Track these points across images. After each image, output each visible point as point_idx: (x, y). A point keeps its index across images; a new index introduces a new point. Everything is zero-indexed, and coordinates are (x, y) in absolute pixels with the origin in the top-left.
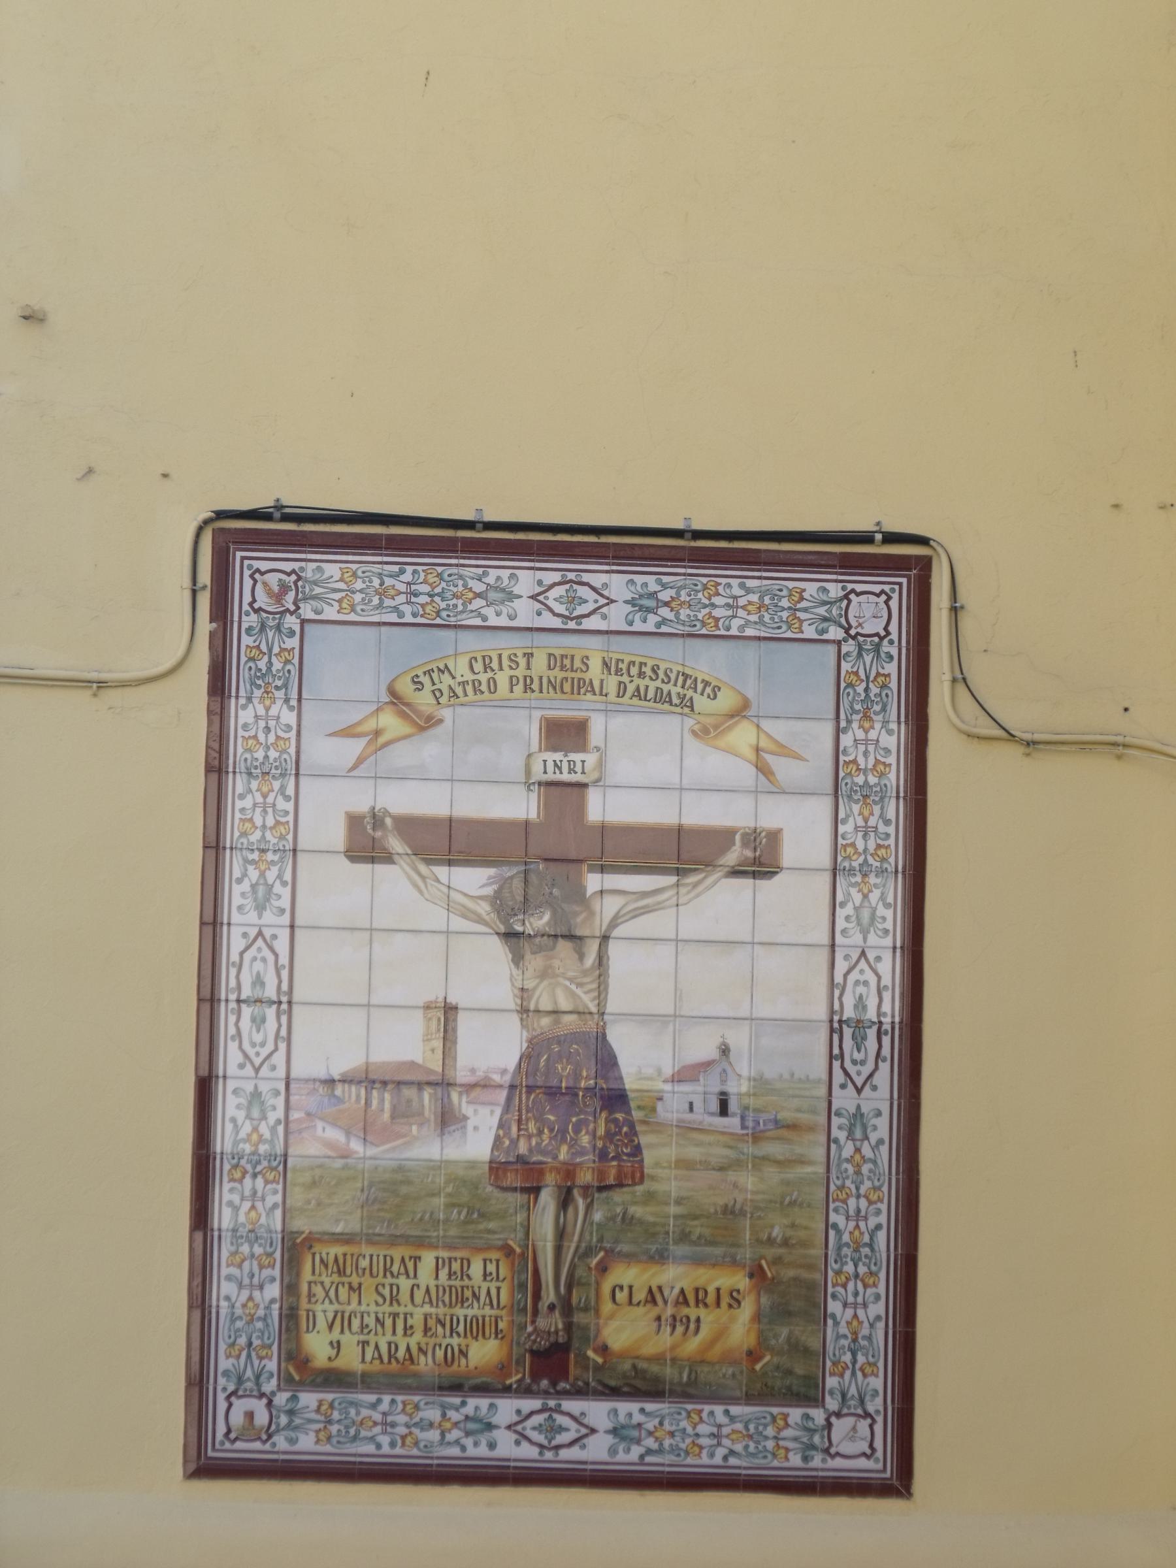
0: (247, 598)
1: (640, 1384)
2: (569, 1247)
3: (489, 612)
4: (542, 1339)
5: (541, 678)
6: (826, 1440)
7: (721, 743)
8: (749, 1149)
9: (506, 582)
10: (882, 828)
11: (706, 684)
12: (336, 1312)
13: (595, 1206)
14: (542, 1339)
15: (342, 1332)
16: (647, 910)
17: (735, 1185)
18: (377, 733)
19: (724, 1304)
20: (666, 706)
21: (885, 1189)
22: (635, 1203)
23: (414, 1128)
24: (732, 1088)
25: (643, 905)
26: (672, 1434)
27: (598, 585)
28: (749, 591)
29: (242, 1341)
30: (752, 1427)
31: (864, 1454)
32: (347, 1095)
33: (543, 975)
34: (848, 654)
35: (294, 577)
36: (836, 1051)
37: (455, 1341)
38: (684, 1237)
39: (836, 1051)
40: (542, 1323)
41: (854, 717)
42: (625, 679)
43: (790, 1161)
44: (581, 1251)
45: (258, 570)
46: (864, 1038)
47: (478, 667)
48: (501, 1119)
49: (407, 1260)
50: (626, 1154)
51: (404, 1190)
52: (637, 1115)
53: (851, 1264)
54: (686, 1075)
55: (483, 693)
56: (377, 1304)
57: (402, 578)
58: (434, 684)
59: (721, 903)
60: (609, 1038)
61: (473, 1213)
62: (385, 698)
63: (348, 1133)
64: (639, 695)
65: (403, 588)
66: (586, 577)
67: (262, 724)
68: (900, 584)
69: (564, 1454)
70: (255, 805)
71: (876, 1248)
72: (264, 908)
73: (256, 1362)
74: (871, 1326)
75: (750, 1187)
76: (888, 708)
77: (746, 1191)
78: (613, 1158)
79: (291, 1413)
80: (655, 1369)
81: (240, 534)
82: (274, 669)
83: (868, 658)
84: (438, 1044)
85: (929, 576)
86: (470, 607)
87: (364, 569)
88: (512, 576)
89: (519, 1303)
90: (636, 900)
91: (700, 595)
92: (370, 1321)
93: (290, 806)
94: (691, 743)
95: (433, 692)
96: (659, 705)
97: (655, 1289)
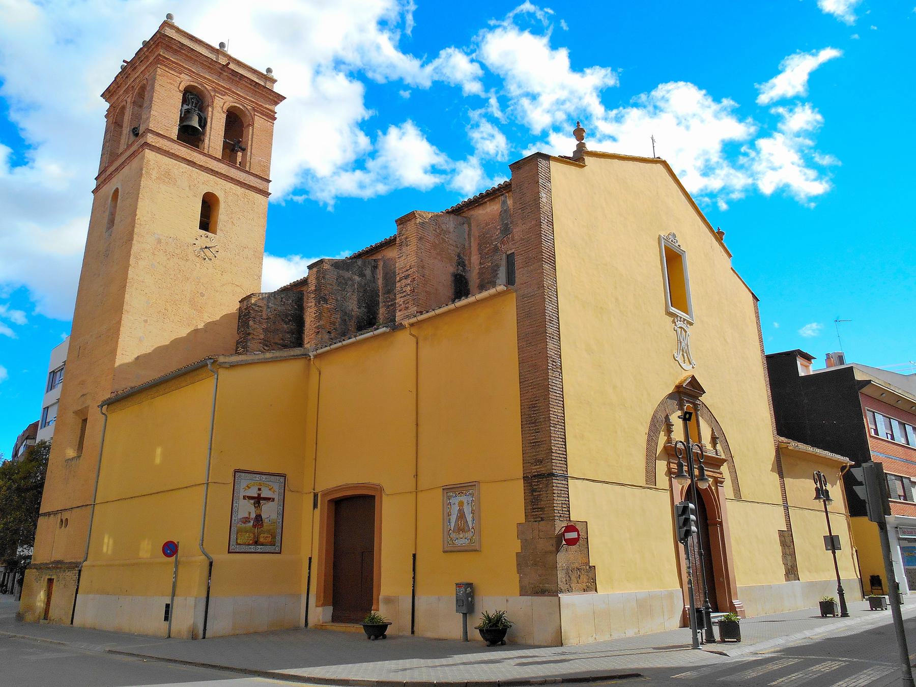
59: (271, 504)
81: (236, 471)
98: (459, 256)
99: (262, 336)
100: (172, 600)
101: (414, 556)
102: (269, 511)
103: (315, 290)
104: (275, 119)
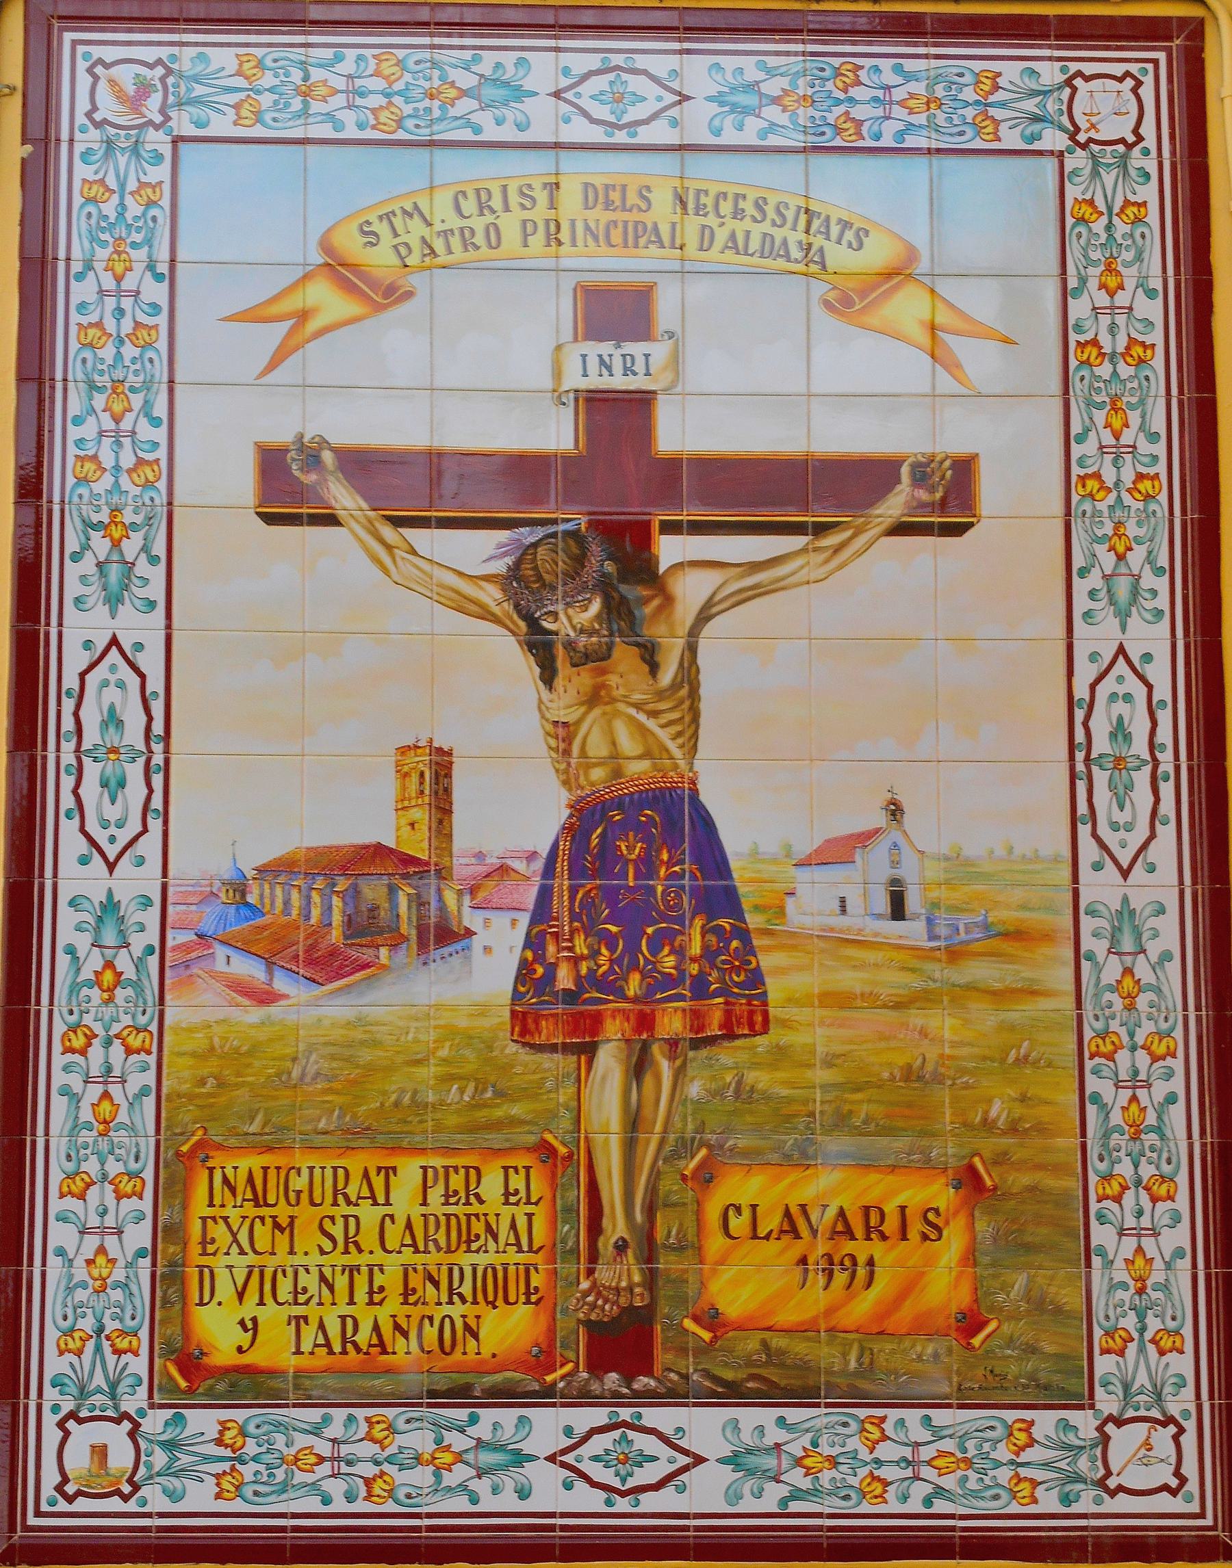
0: (83, 105)
1: (778, 1381)
2: (648, 1141)
3: (484, 119)
4: (606, 1301)
5: (573, 222)
6: (1099, 1463)
7: (873, 320)
8: (940, 972)
9: (511, 70)
10: (1144, 447)
11: (846, 225)
12: (251, 1268)
13: (690, 1072)
14: (606, 1301)
15: (261, 1303)
16: (758, 592)
17: (923, 1033)
18: (303, 316)
19: (914, 1234)
20: (781, 264)
21: (1178, 1034)
22: (755, 1066)
23: (384, 952)
24: (909, 872)
25: (754, 585)
26: (833, 1462)
27: (662, 74)
28: (909, 77)
29: (87, 1324)
30: (970, 1444)
31: (1165, 1488)
32: (267, 901)
33: (595, 698)
34: (1074, 172)
35: (160, 71)
36: (1082, 808)
37: (457, 1310)
38: (841, 1122)
39: (1082, 808)
40: (604, 1274)
41: (1092, 271)
42: (712, 220)
43: (1013, 991)
44: (668, 1148)
45: (100, 61)
46: (1129, 787)
47: (469, 206)
48: (528, 934)
49: (373, 1173)
50: (737, 985)
51: (366, 1056)
52: (753, 920)
53: (1127, 1161)
54: (839, 851)
55: (478, 248)
56: (322, 1252)
57: (339, 68)
58: (396, 235)
59: (886, 573)
60: (704, 798)
61: (484, 1090)
62: (317, 258)
63: (270, 965)
64: (736, 247)
65: (340, 83)
66: (641, 61)
67: (110, 303)
68: (1155, 62)
69: (650, 1502)
70: (101, 434)
71: (1168, 1133)
72: (120, 600)
73: (111, 1359)
74: (1168, 1266)
75: (947, 1035)
76: (1146, 255)
77: (942, 1041)
78: (716, 994)
79: (171, 1446)
80: (799, 1348)
82: (129, 216)
83: (1109, 178)
84: (421, 815)
85: (1202, 50)
86: (453, 112)
87: (276, 55)
88: (520, 62)
89: (564, 1241)
90: (742, 576)
91: (829, 85)
92: (310, 1281)
93: (161, 435)
94: (825, 321)
95: (395, 247)
96: (768, 262)
97: (794, 1210)
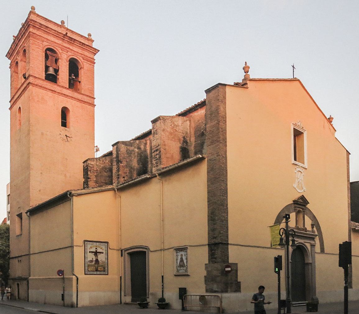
59: (102, 254)
81: (85, 241)
98: (184, 138)
99: (95, 179)
100: (64, 292)
101: (163, 276)
102: (101, 258)
103: (116, 157)
104: (95, 63)
